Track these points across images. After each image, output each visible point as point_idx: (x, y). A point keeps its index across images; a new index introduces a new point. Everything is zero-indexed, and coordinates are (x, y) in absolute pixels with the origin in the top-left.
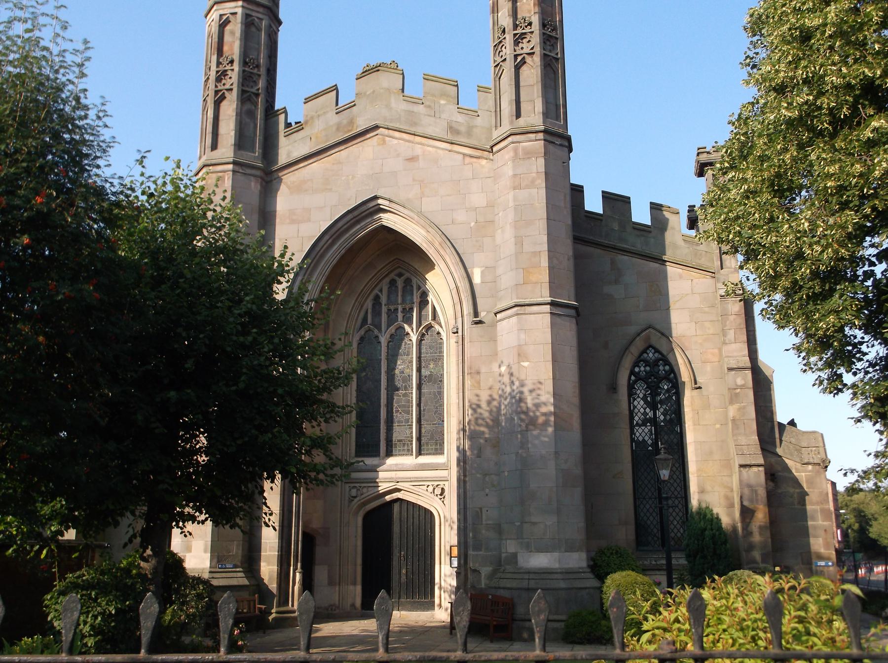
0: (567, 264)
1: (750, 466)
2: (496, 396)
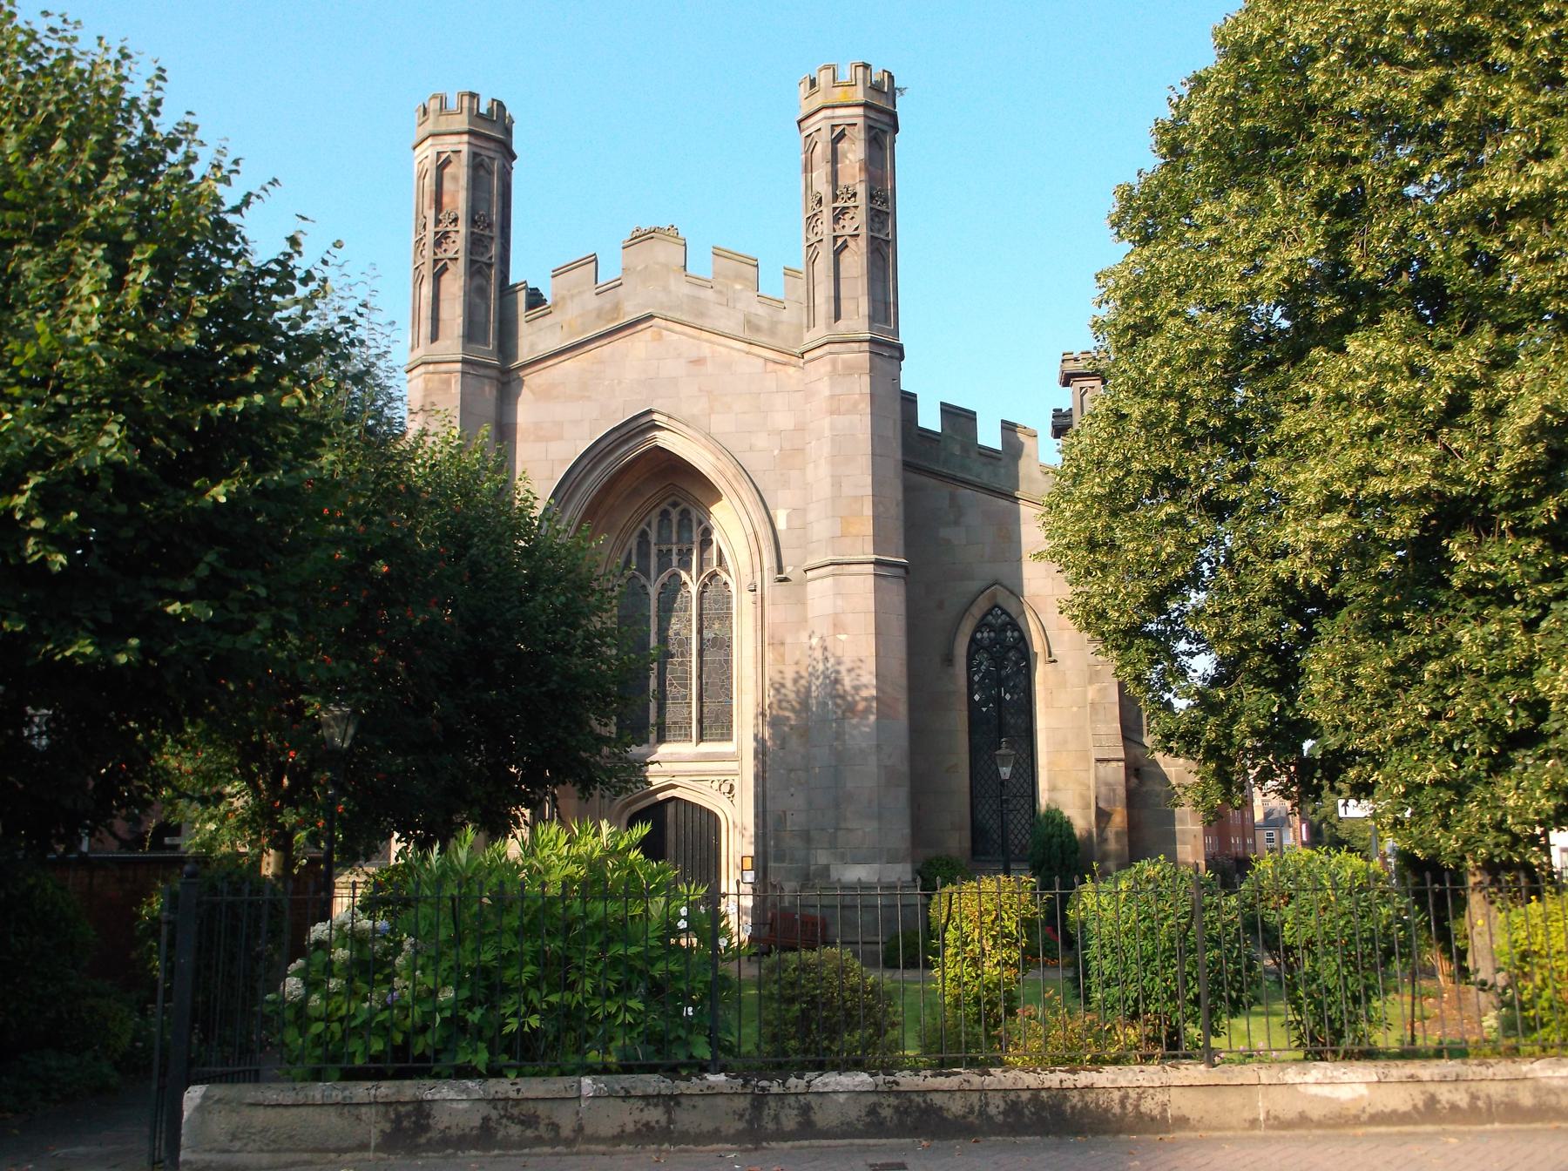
0: (895, 511)
1: (1108, 761)
2: (804, 674)
